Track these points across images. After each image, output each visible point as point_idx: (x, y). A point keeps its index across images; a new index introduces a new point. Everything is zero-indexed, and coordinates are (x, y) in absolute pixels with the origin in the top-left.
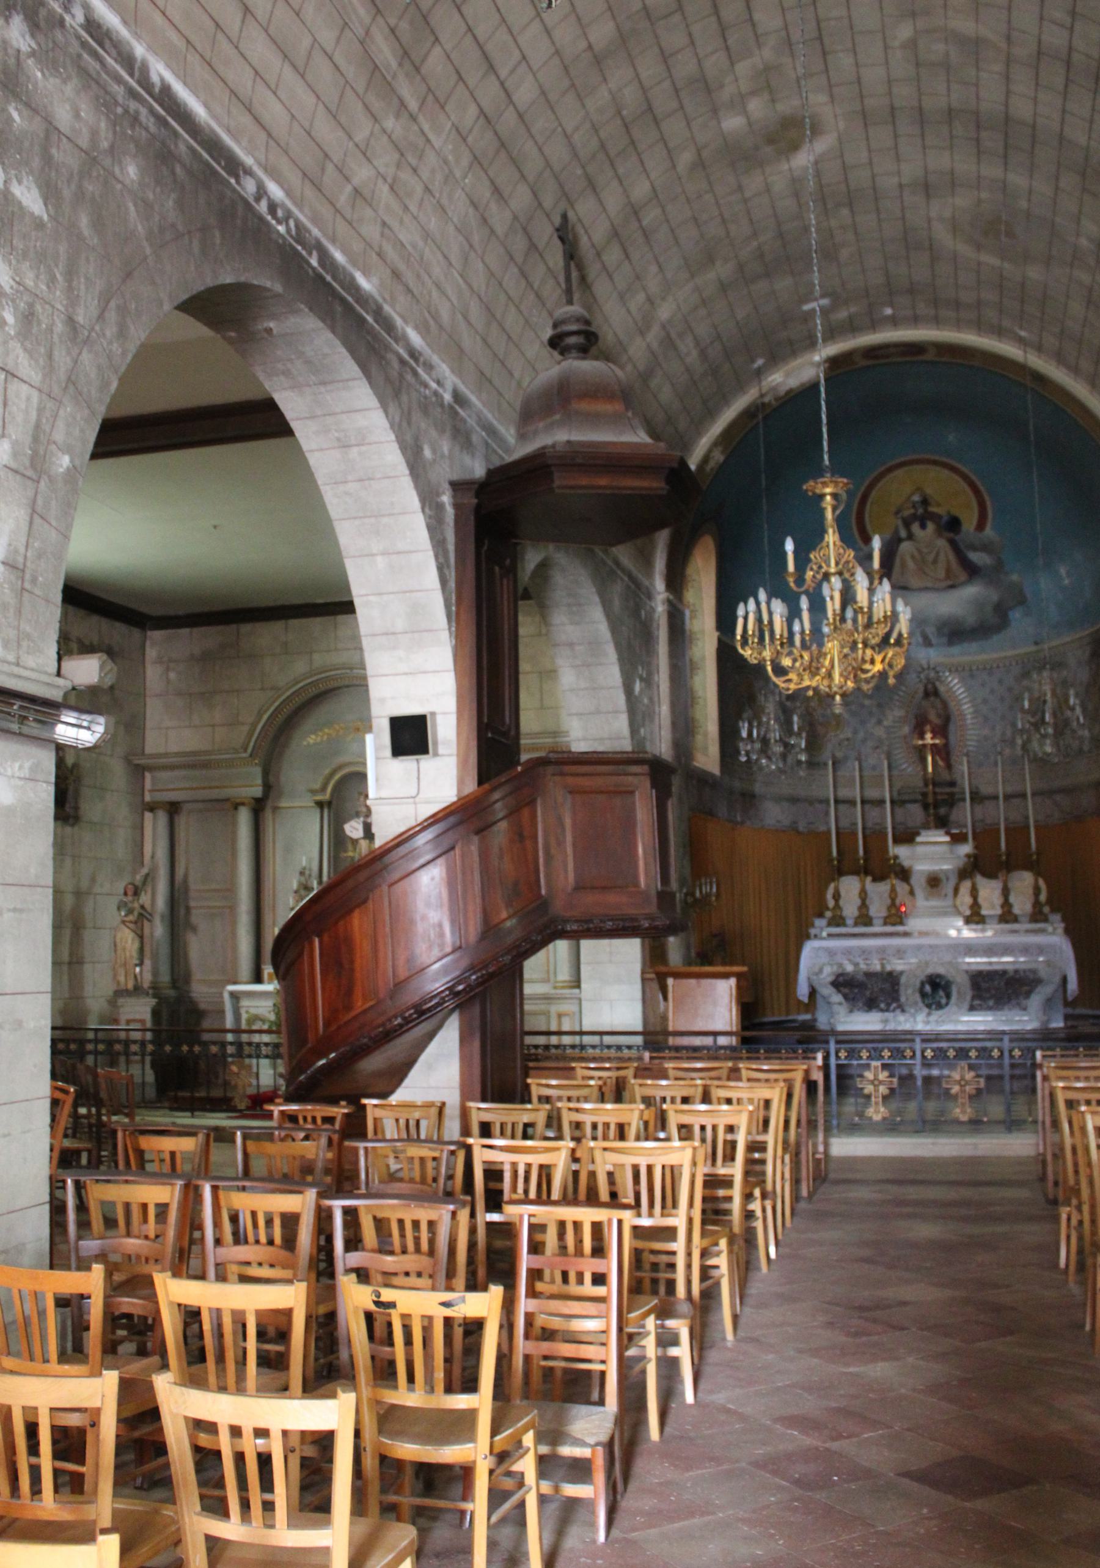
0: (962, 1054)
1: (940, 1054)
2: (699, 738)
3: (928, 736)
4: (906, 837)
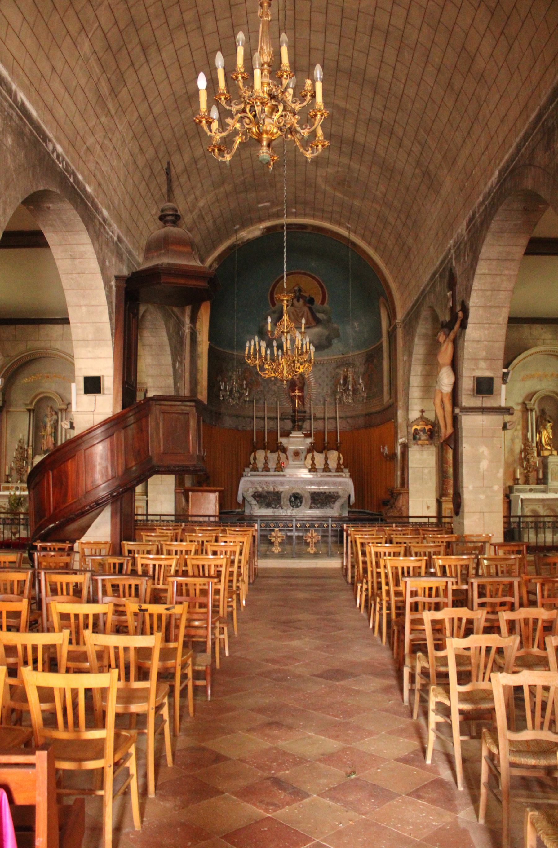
0: (312, 526)
1: (303, 526)
2: (199, 387)
3: (297, 391)
4: (286, 434)
